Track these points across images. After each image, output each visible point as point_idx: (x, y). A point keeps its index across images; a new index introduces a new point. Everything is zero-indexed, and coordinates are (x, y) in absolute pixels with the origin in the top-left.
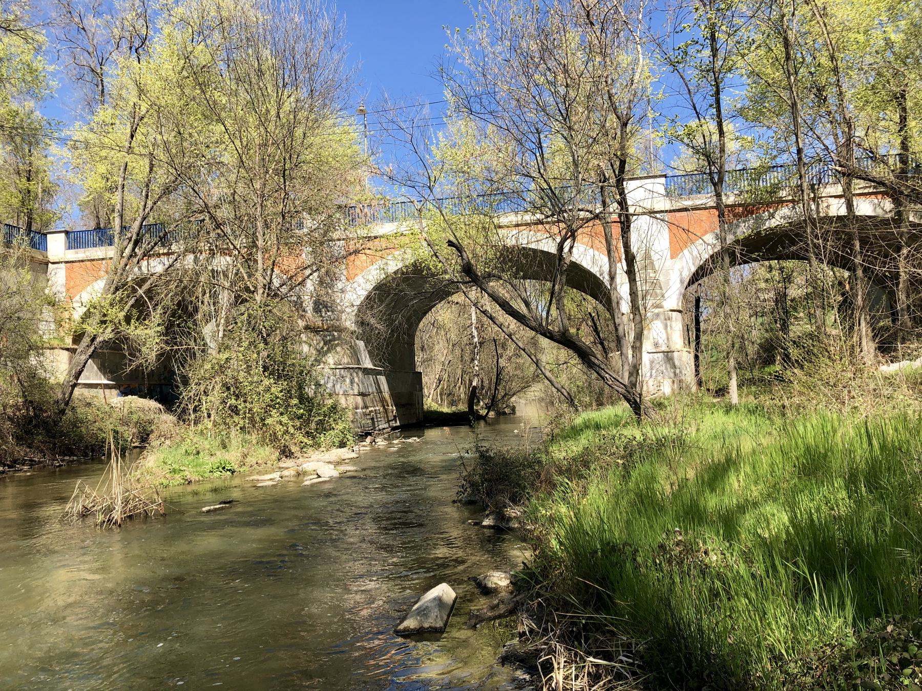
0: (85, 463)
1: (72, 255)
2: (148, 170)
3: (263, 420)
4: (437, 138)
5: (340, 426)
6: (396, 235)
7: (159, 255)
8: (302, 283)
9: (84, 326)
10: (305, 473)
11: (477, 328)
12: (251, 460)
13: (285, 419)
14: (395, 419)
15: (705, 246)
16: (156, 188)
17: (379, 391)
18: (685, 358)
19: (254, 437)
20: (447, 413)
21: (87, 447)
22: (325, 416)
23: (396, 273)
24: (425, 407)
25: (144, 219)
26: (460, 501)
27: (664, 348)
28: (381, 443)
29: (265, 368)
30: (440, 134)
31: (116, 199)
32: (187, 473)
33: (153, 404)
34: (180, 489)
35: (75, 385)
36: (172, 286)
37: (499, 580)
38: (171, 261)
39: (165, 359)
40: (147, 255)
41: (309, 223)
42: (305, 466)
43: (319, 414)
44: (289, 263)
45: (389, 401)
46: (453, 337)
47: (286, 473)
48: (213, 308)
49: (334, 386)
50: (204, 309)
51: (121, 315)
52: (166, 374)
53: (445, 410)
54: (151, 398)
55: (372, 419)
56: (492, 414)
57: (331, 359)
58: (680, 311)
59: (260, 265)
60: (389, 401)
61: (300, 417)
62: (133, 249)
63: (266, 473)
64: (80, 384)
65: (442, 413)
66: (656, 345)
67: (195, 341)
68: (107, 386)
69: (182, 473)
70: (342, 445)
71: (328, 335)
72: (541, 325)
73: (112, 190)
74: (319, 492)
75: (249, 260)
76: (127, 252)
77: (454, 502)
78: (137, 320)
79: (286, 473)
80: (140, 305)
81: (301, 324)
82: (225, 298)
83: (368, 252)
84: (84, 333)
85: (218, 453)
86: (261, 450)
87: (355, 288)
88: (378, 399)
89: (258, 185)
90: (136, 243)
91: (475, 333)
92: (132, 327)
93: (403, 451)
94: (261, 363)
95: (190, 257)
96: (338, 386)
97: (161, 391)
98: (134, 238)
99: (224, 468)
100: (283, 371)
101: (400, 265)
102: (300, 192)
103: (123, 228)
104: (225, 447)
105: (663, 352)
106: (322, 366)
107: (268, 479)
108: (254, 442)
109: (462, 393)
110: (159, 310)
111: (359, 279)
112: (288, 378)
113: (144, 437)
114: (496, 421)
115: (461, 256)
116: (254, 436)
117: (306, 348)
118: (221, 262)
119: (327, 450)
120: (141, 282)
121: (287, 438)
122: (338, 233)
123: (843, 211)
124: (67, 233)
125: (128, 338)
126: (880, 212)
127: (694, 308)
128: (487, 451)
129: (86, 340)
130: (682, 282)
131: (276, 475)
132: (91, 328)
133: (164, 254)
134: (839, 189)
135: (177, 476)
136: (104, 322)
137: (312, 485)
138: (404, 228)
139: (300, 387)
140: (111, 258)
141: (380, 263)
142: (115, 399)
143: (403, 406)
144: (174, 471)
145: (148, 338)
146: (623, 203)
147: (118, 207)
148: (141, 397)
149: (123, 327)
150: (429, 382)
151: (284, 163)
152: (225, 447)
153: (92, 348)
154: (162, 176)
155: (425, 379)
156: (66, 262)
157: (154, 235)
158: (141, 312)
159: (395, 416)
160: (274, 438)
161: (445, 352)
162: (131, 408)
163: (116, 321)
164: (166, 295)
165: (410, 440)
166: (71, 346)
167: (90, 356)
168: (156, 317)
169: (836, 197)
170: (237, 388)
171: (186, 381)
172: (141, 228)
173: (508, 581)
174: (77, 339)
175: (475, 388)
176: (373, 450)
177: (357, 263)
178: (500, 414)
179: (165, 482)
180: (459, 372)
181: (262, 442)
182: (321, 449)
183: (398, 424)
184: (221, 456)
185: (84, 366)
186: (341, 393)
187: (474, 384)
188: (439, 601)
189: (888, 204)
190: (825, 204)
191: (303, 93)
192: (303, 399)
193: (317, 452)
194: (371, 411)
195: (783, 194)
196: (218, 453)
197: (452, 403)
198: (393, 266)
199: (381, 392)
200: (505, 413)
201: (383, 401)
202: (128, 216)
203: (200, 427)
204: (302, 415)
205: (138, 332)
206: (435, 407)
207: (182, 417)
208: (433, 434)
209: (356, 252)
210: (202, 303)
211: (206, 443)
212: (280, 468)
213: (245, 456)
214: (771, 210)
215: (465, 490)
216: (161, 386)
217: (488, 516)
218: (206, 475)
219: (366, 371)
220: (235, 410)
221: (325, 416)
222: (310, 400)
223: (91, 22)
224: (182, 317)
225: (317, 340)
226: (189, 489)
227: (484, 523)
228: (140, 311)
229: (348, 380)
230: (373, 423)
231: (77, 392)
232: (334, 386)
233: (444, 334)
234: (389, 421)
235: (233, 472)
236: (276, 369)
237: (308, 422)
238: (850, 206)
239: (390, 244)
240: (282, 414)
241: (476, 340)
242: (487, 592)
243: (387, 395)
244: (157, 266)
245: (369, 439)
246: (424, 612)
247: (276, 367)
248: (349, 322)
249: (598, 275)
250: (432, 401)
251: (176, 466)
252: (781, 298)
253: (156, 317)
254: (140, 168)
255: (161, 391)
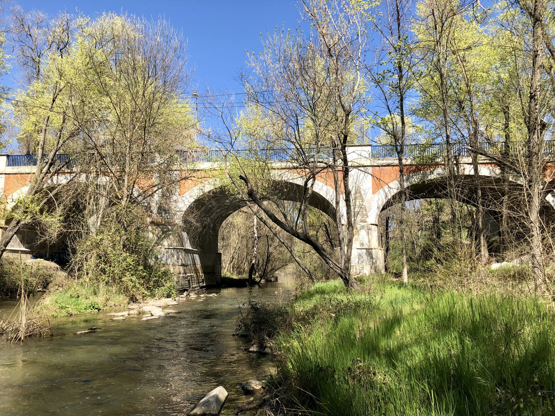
0: (6, 300)
1: (10, 170)
2: (62, 121)
3: (120, 278)
4: (239, 114)
5: (168, 284)
6: (210, 170)
7: (64, 173)
8: (152, 195)
9: (13, 214)
10: (144, 313)
11: (257, 228)
12: (111, 303)
13: (134, 278)
14: (203, 282)
15: (394, 187)
16: (66, 133)
17: (194, 264)
18: (379, 254)
19: (114, 289)
20: (236, 279)
21: (8, 290)
22: (159, 277)
23: (209, 192)
24: (222, 275)
25: (57, 151)
26: (238, 335)
27: (366, 247)
28: (193, 296)
29: (124, 246)
30: (241, 112)
31: (41, 137)
32: (70, 309)
33: (53, 265)
34: (64, 319)
35: (4, 250)
36: (71, 193)
37: (256, 385)
38: (72, 177)
39: (63, 237)
40: (57, 172)
41: (158, 159)
42: (144, 308)
43: (156, 276)
44: (144, 183)
45: (200, 271)
46: (242, 232)
47: (132, 312)
48: (95, 207)
49: (167, 260)
50: (89, 207)
51: (38, 208)
52: (63, 246)
53: (235, 277)
54: (52, 261)
55: (189, 281)
56: (263, 281)
57: (166, 243)
58: (376, 225)
59: (126, 183)
60: (200, 271)
61: (144, 278)
62: (49, 169)
63: (120, 311)
64: (7, 250)
65: (233, 279)
66: (362, 244)
67: (82, 227)
68: (23, 252)
69: (66, 309)
70: (169, 296)
71: (164, 228)
72: (292, 229)
73: (38, 132)
74: (149, 326)
75: (120, 179)
76: (45, 170)
77: (233, 335)
78: (47, 212)
79: (132, 312)
80: (50, 203)
81: (149, 220)
82: (103, 202)
83: (193, 178)
84: (13, 218)
85: (91, 297)
86: (118, 297)
87: (184, 200)
88: (193, 268)
89: (128, 135)
90: (51, 165)
91: (256, 231)
92: (44, 216)
93: (207, 302)
94: (122, 243)
95: (84, 176)
96: (169, 261)
97: (59, 256)
98: (50, 162)
99: (93, 307)
100: (135, 248)
101: (212, 188)
102: (154, 141)
103: (44, 155)
104: (95, 294)
105: (366, 249)
106: (160, 246)
107: (120, 316)
108: (114, 291)
109: (246, 267)
110: (62, 207)
111: (187, 195)
112: (137, 253)
113: (46, 285)
114: (265, 286)
115: (247, 185)
116: (114, 288)
117: (151, 235)
118: (103, 180)
119: (159, 299)
120: (52, 189)
121: (134, 290)
122: (176, 166)
123: (472, 173)
124: (8, 156)
125: (41, 223)
126: (493, 175)
127: (385, 224)
128: (256, 305)
129: (14, 223)
130: (378, 208)
131: (126, 313)
132: (17, 216)
133: (68, 173)
134: (470, 160)
135: (63, 311)
136: (26, 212)
137: (147, 320)
138: (216, 165)
139: (145, 259)
140: (34, 173)
141: (200, 186)
142: (29, 260)
143: (209, 273)
144: (62, 308)
145: (53, 224)
146: (345, 160)
147: (41, 143)
148: (46, 259)
149: (38, 216)
150: (226, 259)
151: (145, 121)
152: (95, 294)
153: (17, 228)
154: (70, 126)
155: (223, 258)
156: (5, 174)
157: (63, 161)
158: (50, 207)
159: (203, 280)
160: (126, 290)
161: (237, 242)
162: (39, 266)
163: (34, 212)
164: (66, 198)
165: (211, 295)
166: (4, 226)
167: (15, 233)
168: (59, 211)
169: (468, 164)
170: (106, 257)
171: (74, 252)
172: (54, 156)
173: (261, 386)
174: (8, 222)
175: (253, 264)
176: (188, 300)
177: (186, 185)
178: (268, 281)
179: (55, 314)
180: (245, 254)
181: (119, 292)
182: (156, 298)
183: (204, 285)
184: (93, 299)
185: (11, 239)
186: (171, 264)
187: (253, 262)
188: (217, 398)
189: (498, 171)
190: (462, 168)
191: (160, 83)
192: (147, 267)
193: (153, 300)
194: (189, 276)
195: (439, 160)
196: (91, 297)
197: (239, 273)
198: (208, 187)
199: (195, 264)
200: (271, 281)
201: (196, 271)
202: (47, 148)
203: (81, 280)
204: (145, 276)
205: (47, 219)
206: (228, 275)
207: (71, 273)
208: (227, 292)
209: (186, 178)
210: (89, 204)
211: (84, 290)
212: (129, 309)
213: (107, 300)
214: (432, 169)
215: (241, 328)
216: (59, 253)
217: (253, 345)
218: (82, 311)
219: (187, 251)
220: (104, 271)
221: (159, 277)
222: (150, 267)
223: (35, 31)
224: (76, 211)
225: (158, 231)
226: (71, 319)
227: (251, 350)
228: (50, 207)
229: (175, 257)
230: (189, 283)
231: (5, 255)
232: (167, 260)
233: (237, 228)
234: (199, 283)
235: (99, 310)
236: (131, 247)
237: (148, 281)
238: (476, 170)
239: (207, 175)
240: (132, 275)
241: (256, 235)
242: (249, 392)
243: (199, 266)
244: (63, 180)
245: (185, 293)
246: (207, 403)
247: (131, 246)
248: (178, 220)
249: (330, 201)
250: (227, 271)
251: (63, 305)
252: (436, 220)
253: (59, 211)
254: (57, 120)
255: (59, 256)
